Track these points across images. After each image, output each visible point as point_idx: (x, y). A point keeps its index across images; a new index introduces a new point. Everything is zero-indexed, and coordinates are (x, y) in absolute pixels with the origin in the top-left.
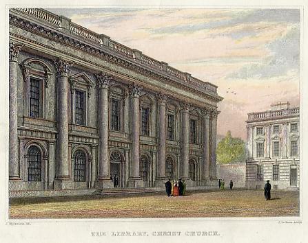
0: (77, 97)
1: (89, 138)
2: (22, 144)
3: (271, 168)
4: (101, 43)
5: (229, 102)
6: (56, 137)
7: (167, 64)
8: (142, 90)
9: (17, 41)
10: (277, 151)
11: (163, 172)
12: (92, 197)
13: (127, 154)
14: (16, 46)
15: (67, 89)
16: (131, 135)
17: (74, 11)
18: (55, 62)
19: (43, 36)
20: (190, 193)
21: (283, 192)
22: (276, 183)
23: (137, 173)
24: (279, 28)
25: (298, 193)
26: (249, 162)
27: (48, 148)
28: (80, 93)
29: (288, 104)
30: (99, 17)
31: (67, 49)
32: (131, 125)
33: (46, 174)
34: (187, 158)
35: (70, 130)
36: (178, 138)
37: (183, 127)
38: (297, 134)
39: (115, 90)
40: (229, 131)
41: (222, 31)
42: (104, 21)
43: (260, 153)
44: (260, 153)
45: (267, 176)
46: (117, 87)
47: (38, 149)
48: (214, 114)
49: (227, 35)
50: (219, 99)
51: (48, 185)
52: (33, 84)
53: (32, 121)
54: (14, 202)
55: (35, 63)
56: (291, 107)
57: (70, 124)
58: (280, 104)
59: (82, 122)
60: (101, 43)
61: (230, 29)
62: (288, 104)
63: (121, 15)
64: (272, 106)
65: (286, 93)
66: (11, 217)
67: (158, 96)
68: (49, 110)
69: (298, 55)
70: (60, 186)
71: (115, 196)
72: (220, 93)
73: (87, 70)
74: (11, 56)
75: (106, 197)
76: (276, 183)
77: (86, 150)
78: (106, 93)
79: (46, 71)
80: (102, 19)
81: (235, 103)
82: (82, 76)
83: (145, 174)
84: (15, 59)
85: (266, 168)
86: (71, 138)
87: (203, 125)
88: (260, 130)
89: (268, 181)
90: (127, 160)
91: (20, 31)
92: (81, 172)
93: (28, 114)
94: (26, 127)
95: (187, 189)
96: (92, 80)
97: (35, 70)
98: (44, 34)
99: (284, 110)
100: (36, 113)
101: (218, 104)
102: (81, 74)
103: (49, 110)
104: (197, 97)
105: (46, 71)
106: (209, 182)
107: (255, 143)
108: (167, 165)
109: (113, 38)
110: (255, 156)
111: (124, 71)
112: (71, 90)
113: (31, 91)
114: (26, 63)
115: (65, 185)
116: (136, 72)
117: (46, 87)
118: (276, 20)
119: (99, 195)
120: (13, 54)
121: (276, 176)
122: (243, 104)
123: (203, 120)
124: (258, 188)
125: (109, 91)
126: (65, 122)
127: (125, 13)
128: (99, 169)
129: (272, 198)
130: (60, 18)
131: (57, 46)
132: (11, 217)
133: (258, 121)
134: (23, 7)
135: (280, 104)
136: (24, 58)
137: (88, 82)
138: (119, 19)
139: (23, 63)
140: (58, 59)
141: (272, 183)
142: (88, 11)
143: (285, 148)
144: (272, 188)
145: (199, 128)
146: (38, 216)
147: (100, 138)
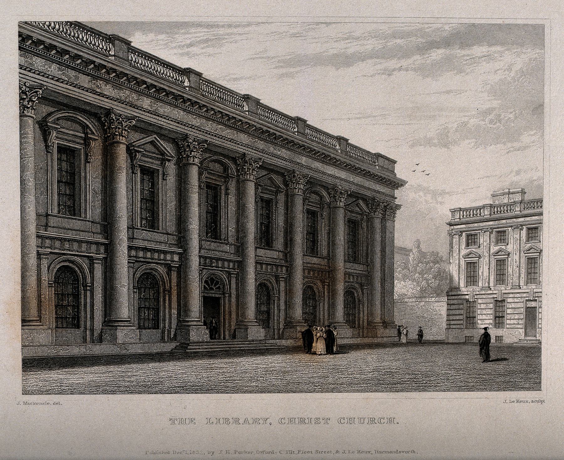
0: (142, 180)
1: (165, 253)
2: (45, 263)
3: (491, 306)
4: (187, 84)
5: (420, 188)
6: (106, 251)
7: (347, 140)
8: (261, 167)
9: (33, 79)
10: (501, 277)
11: (298, 312)
12: (171, 356)
13: (233, 281)
14: (31, 88)
15: (124, 166)
16: (240, 248)
17: (144, 26)
18: (102, 116)
19: (79, 71)
20: (344, 349)
21: (512, 348)
22: (500, 332)
23: (251, 312)
24: (508, 57)
25: (540, 349)
26: (452, 293)
27: (92, 271)
28: (145, 171)
29: (523, 192)
30: (181, 38)
31: (124, 94)
32: (241, 230)
33: (76, 314)
34: (340, 288)
35: (131, 239)
36: (325, 252)
37: (241, 208)
38: (540, 246)
39: (211, 165)
40: (418, 241)
41: (404, 63)
42: (191, 45)
43: (472, 279)
44: (472, 279)
45: (484, 319)
46: (215, 161)
47: (73, 271)
48: (389, 209)
49: (415, 70)
50: (397, 184)
51: (92, 334)
52: (64, 157)
53: (66, 223)
54: (30, 364)
55: (67, 119)
56: (527, 197)
57: (131, 228)
58: (509, 193)
59: (152, 223)
60: (187, 84)
61: (417, 59)
62: (523, 192)
63: (215, 33)
64: (493, 196)
65: (518, 173)
66: (25, 392)
67: (287, 176)
68: (93, 207)
69: (542, 106)
70: (114, 338)
71: (211, 355)
72: (400, 172)
73: (161, 132)
74: (23, 108)
75: (196, 355)
76: (500, 332)
77: (271, 283)
78: (194, 172)
79: (86, 134)
80: (188, 42)
81: (426, 190)
82: (152, 143)
83: (265, 319)
84: (30, 113)
85: (483, 306)
86: (133, 253)
87: (371, 228)
88: (471, 240)
89: (485, 329)
90: (234, 292)
91: (39, 63)
92: (149, 316)
93: (55, 211)
94: (52, 233)
95: (340, 342)
96: (169, 148)
97: (66, 133)
98: (57, 58)
99: (515, 203)
100: (71, 205)
101: (397, 193)
102: (149, 139)
103: (93, 207)
104: (358, 180)
105: (86, 134)
106: (381, 331)
107: (463, 263)
108: (304, 300)
109: (208, 74)
110: (462, 284)
111: (228, 133)
112: (133, 167)
113: (60, 170)
114: (51, 119)
115: (122, 334)
116: (249, 134)
117: (87, 161)
118: (502, 44)
119: (183, 352)
120: (26, 103)
121: (499, 320)
122: (443, 193)
123: (370, 220)
124: (468, 341)
125: (257, 185)
126: (123, 224)
127: (229, 31)
128: (183, 308)
129: (505, 362)
130: (111, 39)
131: (108, 90)
132: (25, 392)
133: (467, 226)
134: (43, 20)
135: (509, 193)
136: (45, 109)
137: (163, 154)
138: (217, 41)
139: (45, 120)
140: (108, 112)
141: (493, 332)
142: (171, 28)
143: (516, 266)
144: (493, 340)
145: (362, 233)
146: (72, 391)
147: (184, 256)
